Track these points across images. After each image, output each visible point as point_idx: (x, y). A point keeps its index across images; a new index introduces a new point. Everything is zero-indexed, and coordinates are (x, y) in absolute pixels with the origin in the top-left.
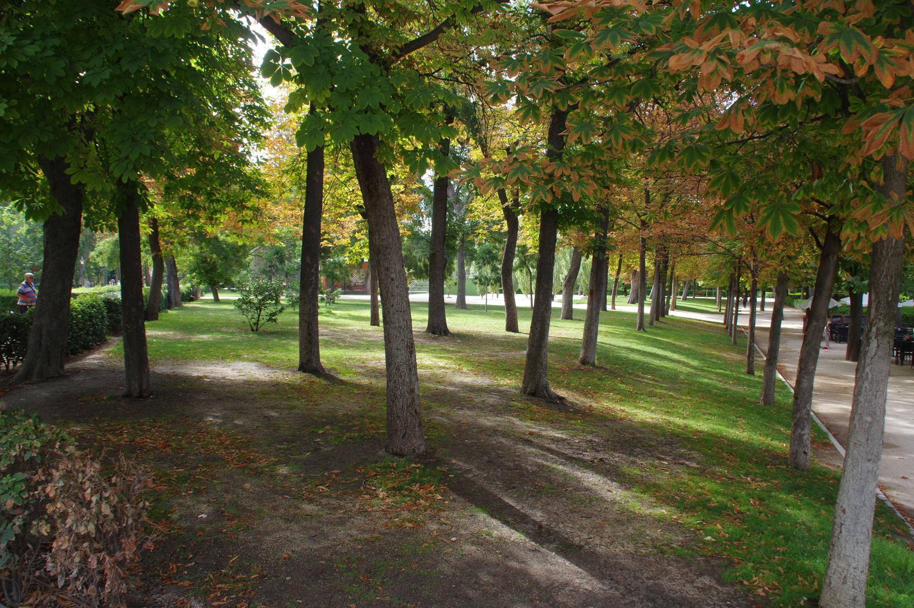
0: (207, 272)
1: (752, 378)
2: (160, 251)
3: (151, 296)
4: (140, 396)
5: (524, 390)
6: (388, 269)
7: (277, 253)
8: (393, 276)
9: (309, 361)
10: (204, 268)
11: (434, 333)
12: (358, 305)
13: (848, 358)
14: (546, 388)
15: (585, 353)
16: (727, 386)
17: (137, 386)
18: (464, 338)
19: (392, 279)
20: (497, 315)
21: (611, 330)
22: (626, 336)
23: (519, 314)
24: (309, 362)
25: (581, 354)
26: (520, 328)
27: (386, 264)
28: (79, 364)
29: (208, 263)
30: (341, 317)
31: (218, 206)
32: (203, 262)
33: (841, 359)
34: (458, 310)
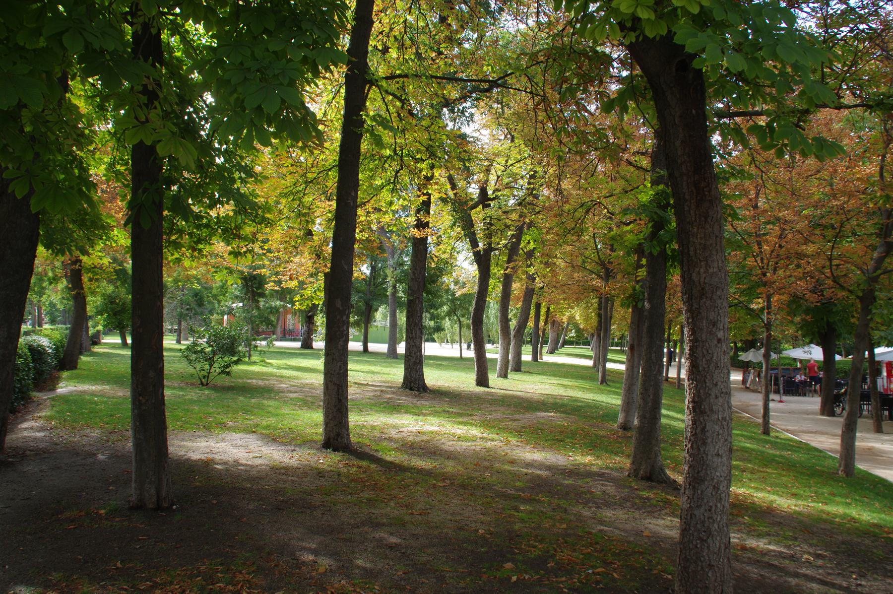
0: (115, 314)
1: (768, 438)
2: (83, 288)
3: (69, 342)
4: (158, 508)
5: (635, 473)
6: (714, 324)
7: (196, 295)
8: (720, 334)
9: (338, 435)
10: (113, 309)
11: (411, 389)
12: (282, 353)
13: (822, 414)
14: (662, 470)
15: (626, 417)
16: (764, 449)
17: (153, 491)
18: (440, 394)
19: (719, 340)
20: (467, 369)
21: (576, 384)
22: (590, 390)
23: (425, 362)
24: (336, 436)
25: (621, 418)
26: (491, 383)
27: (712, 315)
28: (399, 541)
29: (118, 304)
30: (279, 368)
31: (205, 232)
32: (112, 303)
33: (816, 414)
34: (390, 360)
